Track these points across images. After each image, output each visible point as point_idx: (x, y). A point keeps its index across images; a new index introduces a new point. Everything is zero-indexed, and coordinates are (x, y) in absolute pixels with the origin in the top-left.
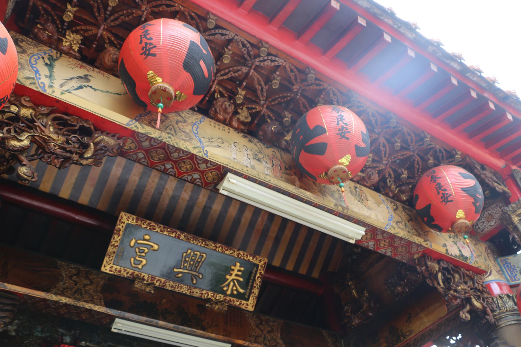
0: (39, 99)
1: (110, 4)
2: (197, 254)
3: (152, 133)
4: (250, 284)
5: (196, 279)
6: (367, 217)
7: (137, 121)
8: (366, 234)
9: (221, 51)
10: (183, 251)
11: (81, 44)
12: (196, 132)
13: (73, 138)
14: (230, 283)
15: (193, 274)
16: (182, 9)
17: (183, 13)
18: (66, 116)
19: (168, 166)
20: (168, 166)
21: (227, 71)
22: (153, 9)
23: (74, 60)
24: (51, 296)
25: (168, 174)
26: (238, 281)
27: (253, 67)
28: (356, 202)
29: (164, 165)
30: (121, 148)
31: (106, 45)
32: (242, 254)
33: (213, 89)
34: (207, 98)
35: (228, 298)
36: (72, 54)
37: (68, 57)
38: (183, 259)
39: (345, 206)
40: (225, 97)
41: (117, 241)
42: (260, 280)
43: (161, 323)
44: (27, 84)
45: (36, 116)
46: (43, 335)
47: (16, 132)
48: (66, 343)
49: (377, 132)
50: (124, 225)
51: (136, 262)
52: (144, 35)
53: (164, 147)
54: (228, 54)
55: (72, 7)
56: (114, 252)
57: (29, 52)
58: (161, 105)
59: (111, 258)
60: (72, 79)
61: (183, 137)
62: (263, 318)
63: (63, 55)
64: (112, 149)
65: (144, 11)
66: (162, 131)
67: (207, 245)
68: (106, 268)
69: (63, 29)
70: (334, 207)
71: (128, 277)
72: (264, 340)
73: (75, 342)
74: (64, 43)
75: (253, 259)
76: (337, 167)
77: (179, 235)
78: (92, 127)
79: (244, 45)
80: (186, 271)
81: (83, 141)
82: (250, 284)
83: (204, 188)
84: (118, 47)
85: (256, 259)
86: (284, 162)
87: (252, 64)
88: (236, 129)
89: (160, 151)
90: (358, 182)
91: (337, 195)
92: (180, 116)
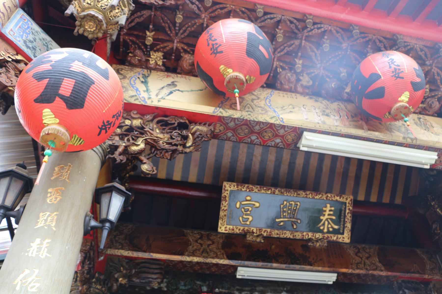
0: (143, 110)
1: (177, 21)
2: (292, 204)
3: (235, 114)
4: (342, 220)
5: (296, 224)
6: (437, 142)
7: (220, 107)
8: (439, 158)
9: (273, 32)
10: (280, 203)
11: (164, 59)
12: (269, 105)
13: (175, 134)
14: (324, 222)
15: (292, 221)
16: (234, 7)
17: (235, 11)
18: (165, 118)
19: (254, 138)
20: (254, 138)
21: (282, 47)
22: (210, 15)
23: (161, 72)
25: (255, 144)
26: (331, 219)
27: (304, 38)
28: (423, 131)
29: (250, 138)
30: (213, 132)
31: (182, 55)
33: (274, 66)
34: (272, 75)
35: (326, 235)
36: (158, 68)
37: (156, 72)
38: (282, 210)
39: (413, 137)
40: (286, 69)
41: (225, 206)
42: (350, 215)
43: (275, 265)
44: (132, 101)
45: (144, 123)
46: (186, 288)
47: (133, 139)
48: (204, 292)
49: (429, 64)
50: (228, 192)
51: (244, 220)
52: (209, 38)
53: (247, 123)
54: (280, 33)
55: (150, 32)
56: (225, 215)
57: (128, 76)
58: (236, 90)
59: (224, 220)
60: (163, 88)
61: (260, 111)
62: (360, 247)
63: (152, 71)
64: (207, 135)
65: (204, 19)
66: (242, 111)
67: (299, 194)
69: (147, 50)
71: (240, 233)
72: (365, 266)
73: (211, 289)
74: (150, 62)
75: (340, 198)
76: (398, 105)
77: (274, 191)
78: (187, 122)
79: (291, 22)
80: (286, 219)
81: (183, 134)
82: (342, 220)
83: (287, 149)
84: (191, 53)
85: (343, 198)
86: (349, 111)
87: (302, 36)
88: (302, 94)
89: (244, 127)
90: (420, 113)
91: (403, 129)
92: (253, 94)
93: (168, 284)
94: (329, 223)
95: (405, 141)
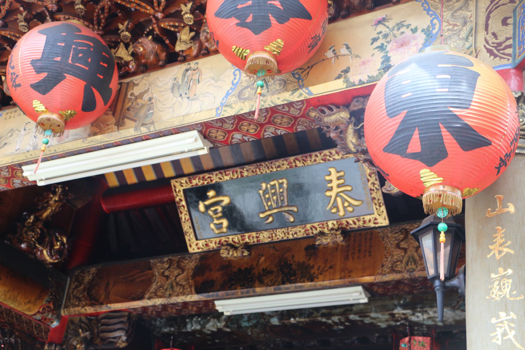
14: (335, 200)
24: (147, 302)
50: (182, 193)
70: (136, 133)
80: (275, 211)
93: (227, 322)
94: (344, 200)
95: (139, 133)
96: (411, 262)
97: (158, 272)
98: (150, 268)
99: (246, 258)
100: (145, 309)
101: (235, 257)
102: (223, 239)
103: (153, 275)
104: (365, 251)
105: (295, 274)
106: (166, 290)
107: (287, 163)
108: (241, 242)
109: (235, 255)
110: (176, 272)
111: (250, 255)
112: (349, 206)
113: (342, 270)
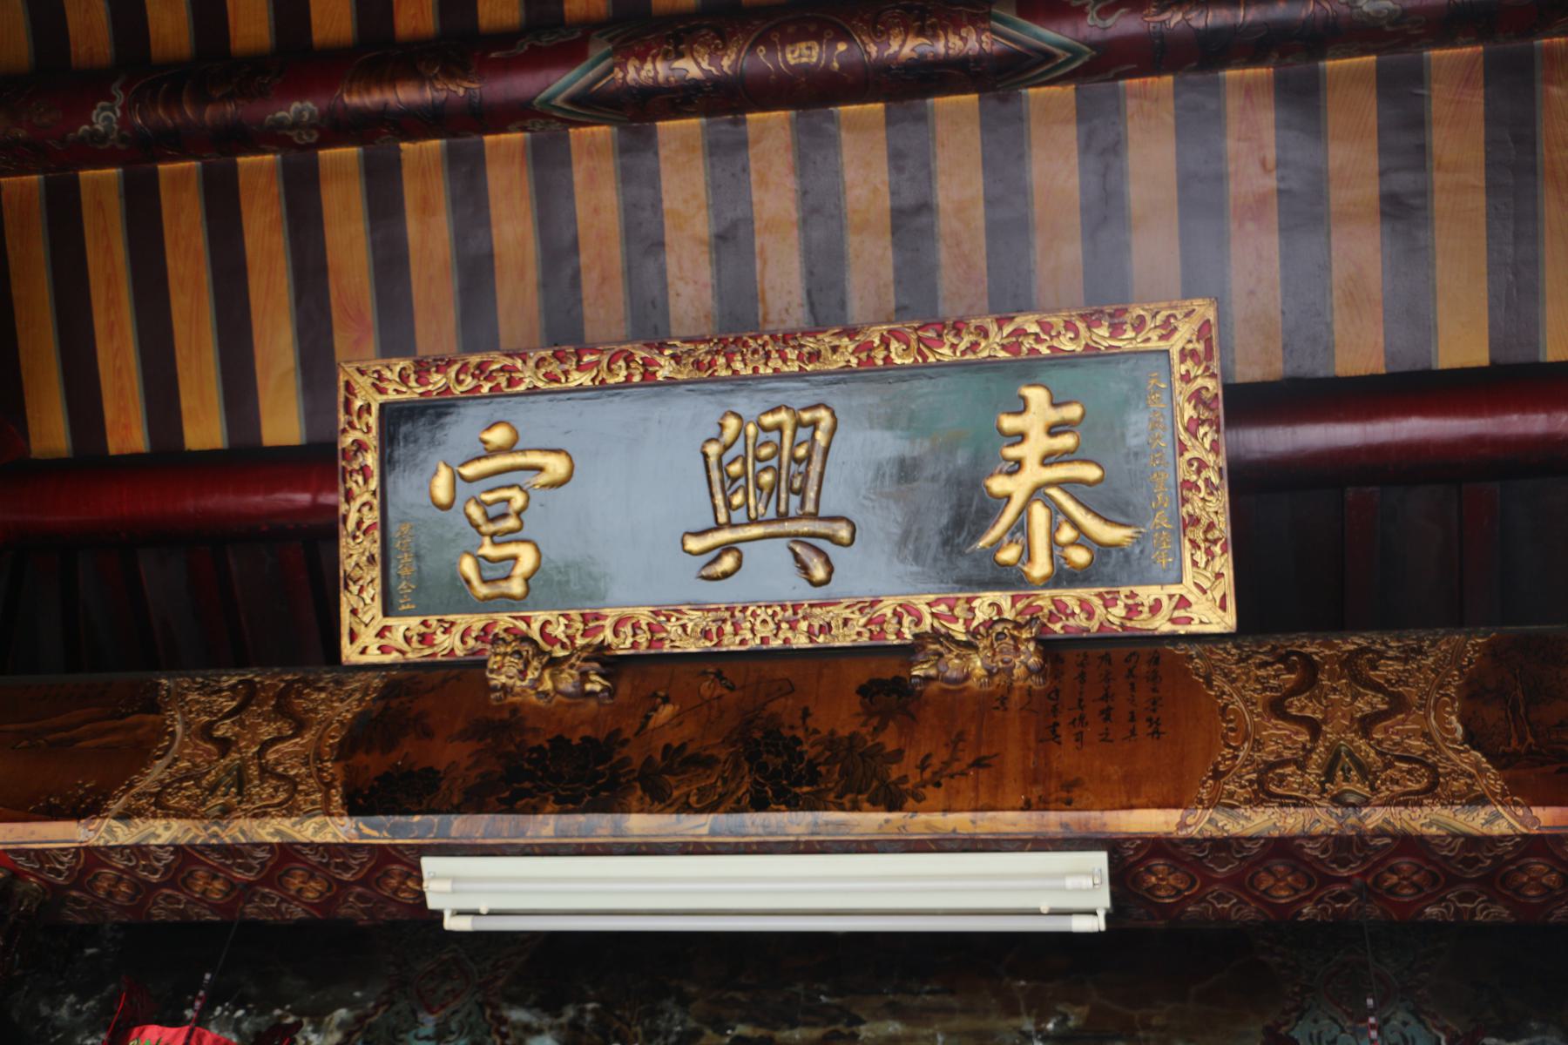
5: (819, 552)
15: (795, 536)
24: (110, 831)
32: (1034, 328)
50: (373, 420)
68: (360, 644)
73: (441, 1034)
75: (1116, 330)
94: (1056, 510)
96: (1346, 771)
97: (187, 725)
98: (154, 707)
99: (592, 703)
100: (93, 857)
101: (546, 694)
102: (504, 620)
103: (162, 731)
104: (1132, 718)
105: (813, 776)
106: (213, 789)
107: (851, 348)
108: (580, 642)
109: (548, 685)
110: (267, 731)
111: (611, 692)
112: (1073, 543)
113: (1033, 777)
